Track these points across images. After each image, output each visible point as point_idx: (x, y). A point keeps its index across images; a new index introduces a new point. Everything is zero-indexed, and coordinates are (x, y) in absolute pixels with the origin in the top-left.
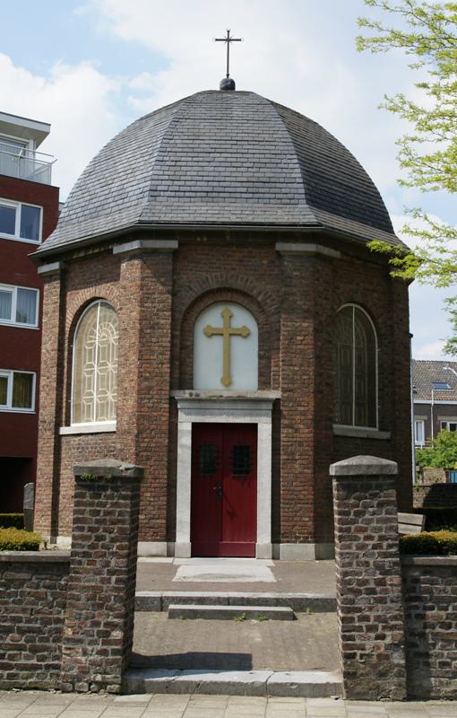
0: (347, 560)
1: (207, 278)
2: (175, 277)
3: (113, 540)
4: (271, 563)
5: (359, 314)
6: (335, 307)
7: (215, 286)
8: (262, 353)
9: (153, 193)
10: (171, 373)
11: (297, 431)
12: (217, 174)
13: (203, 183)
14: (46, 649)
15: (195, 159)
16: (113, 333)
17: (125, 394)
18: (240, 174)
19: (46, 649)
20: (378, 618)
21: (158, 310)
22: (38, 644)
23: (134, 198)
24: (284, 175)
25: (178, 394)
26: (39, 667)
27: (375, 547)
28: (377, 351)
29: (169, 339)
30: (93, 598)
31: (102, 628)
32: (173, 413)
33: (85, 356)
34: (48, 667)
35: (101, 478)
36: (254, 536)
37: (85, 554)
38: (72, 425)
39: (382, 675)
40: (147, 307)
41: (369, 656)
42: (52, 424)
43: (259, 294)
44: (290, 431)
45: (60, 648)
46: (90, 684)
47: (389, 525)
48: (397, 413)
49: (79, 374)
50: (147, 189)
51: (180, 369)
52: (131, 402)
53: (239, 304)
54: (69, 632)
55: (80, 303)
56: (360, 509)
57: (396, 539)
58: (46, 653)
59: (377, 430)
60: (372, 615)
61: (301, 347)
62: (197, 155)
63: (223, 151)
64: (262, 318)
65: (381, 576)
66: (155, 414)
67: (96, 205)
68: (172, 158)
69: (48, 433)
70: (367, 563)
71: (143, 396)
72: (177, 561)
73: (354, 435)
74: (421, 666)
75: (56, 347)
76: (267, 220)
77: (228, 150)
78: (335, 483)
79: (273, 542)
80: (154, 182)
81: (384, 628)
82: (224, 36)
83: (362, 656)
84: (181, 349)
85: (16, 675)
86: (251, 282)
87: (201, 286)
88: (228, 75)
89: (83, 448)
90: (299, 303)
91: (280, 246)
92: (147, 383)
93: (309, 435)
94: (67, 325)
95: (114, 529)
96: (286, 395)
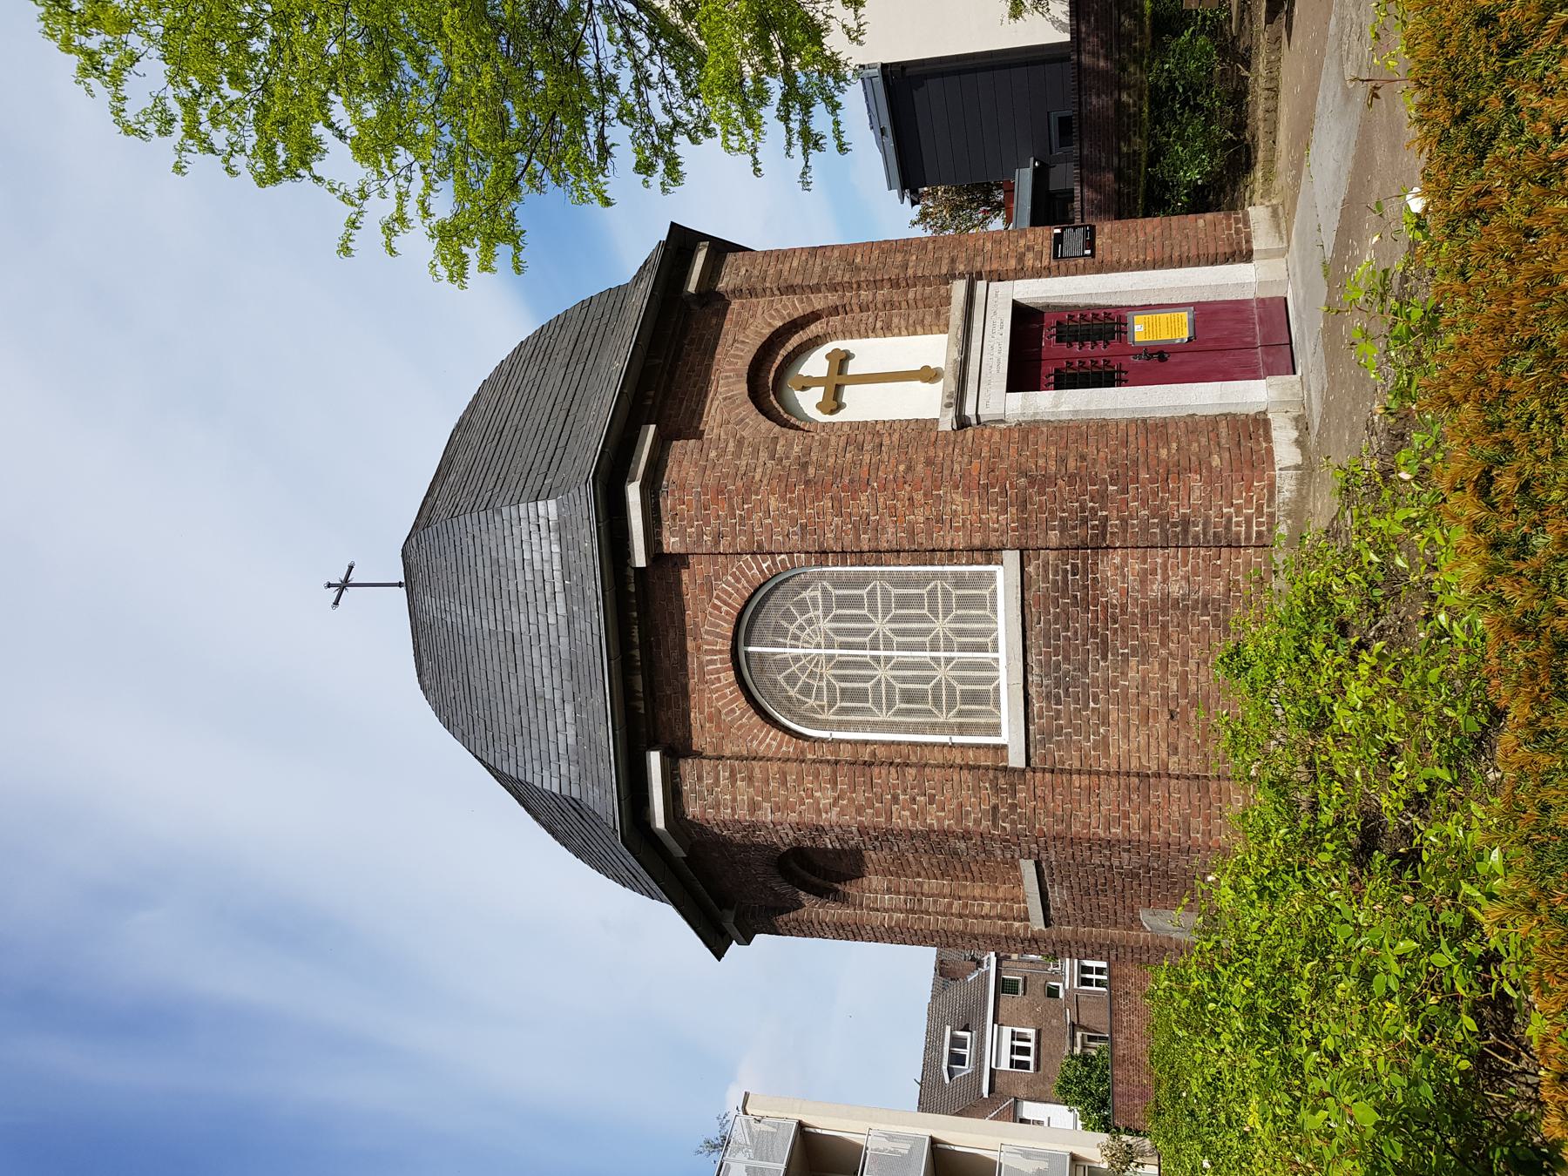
40: (764, 474)
66: (985, 450)
71: (946, 472)
92: (920, 467)
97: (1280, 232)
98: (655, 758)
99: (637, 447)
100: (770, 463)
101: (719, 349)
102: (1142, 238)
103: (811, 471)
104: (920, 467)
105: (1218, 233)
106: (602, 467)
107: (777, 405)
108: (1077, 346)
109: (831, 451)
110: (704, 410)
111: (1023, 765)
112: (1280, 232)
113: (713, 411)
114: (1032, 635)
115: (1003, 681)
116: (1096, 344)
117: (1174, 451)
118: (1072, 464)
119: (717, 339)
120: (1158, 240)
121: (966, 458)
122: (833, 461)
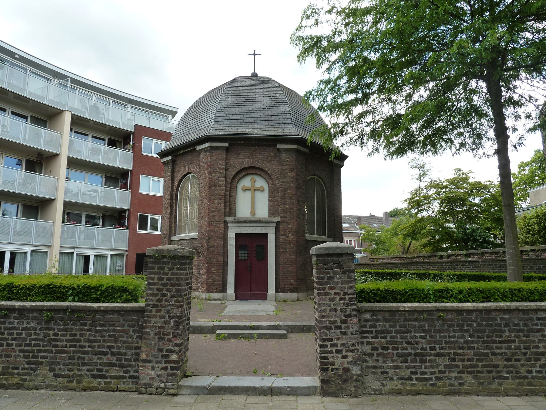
0: (323, 308)
1: (243, 162)
2: (227, 161)
3: (172, 296)
4: (275, 303)
5: (318, 181)
6: (306, 177)
7: (247, 166)
8: (270, 199)
9: (216, 120)
10: (225, 208)
11: (288, 237)
12: (248, 111)
14: (131, 366)
15: (237, 104)
16: (197, 190)
17: (202, 219)
18: (260, 112)
19: (131, 366)
20: (343, 345)
22: (123, 362)
23: (208, 123)
24: (281, 112)
25: (228, 219)
26: (124, 377)
27: (341, 299)
28: (326, 199)
29: (224, 192)
30: (159, 333)
31: (165, 353)
32: (226, 228)
33: (184, 201)
34: (130, 377)
35: (164, 257)
36: (266, 290)
37: (155, 306)
39: (345, 381)
41: (337, 369)
42: (168, 235)
43: (269, 169)
44: (285, 237)
45: (138, 365)
46: (157, 389)
47: (349, 285)
48: (336, 229)
49: (180, 210)
50: (214, 118)
51: (230, 207)
52: (205, 223)
53: (258, 174)
54: (143, 356)
55: (181, 176)
56: (331, 275)
57: (354, 294)
58: (129, 369)
59: (326, 237)
60: (339, 343)
62: (238, 102)
63: (252, 101)
64: (270, 182)
65: (345, 318)
66: (217, 229)
67: (189, 128)
69: (166, 240)
70: (336, 310)
71: (211, 220)
72: (227, 303)
73: (316, 240)
74: (370, 374)
75: (169, 197)
76: (273, 133)
77: (254, 101)
78: (314, 259)
79: (276, 292)
80: (217, 115)
81: (347, 351)
82: (253, 53)
83: (333, 369)
84: (230, 197)
85: (111, 382)
86: (265, 164)
87: (240, 166)
88: (254, 71)
90: (289, 174)
91: (279, 146)
92: (213, 214)
93: (294, 239)
95: (173, 289)
102: (288, 266)
103: (214, 188)
104: (213, 214)
109: (220, 192)
115: (188, 234)
118: (211, 249)
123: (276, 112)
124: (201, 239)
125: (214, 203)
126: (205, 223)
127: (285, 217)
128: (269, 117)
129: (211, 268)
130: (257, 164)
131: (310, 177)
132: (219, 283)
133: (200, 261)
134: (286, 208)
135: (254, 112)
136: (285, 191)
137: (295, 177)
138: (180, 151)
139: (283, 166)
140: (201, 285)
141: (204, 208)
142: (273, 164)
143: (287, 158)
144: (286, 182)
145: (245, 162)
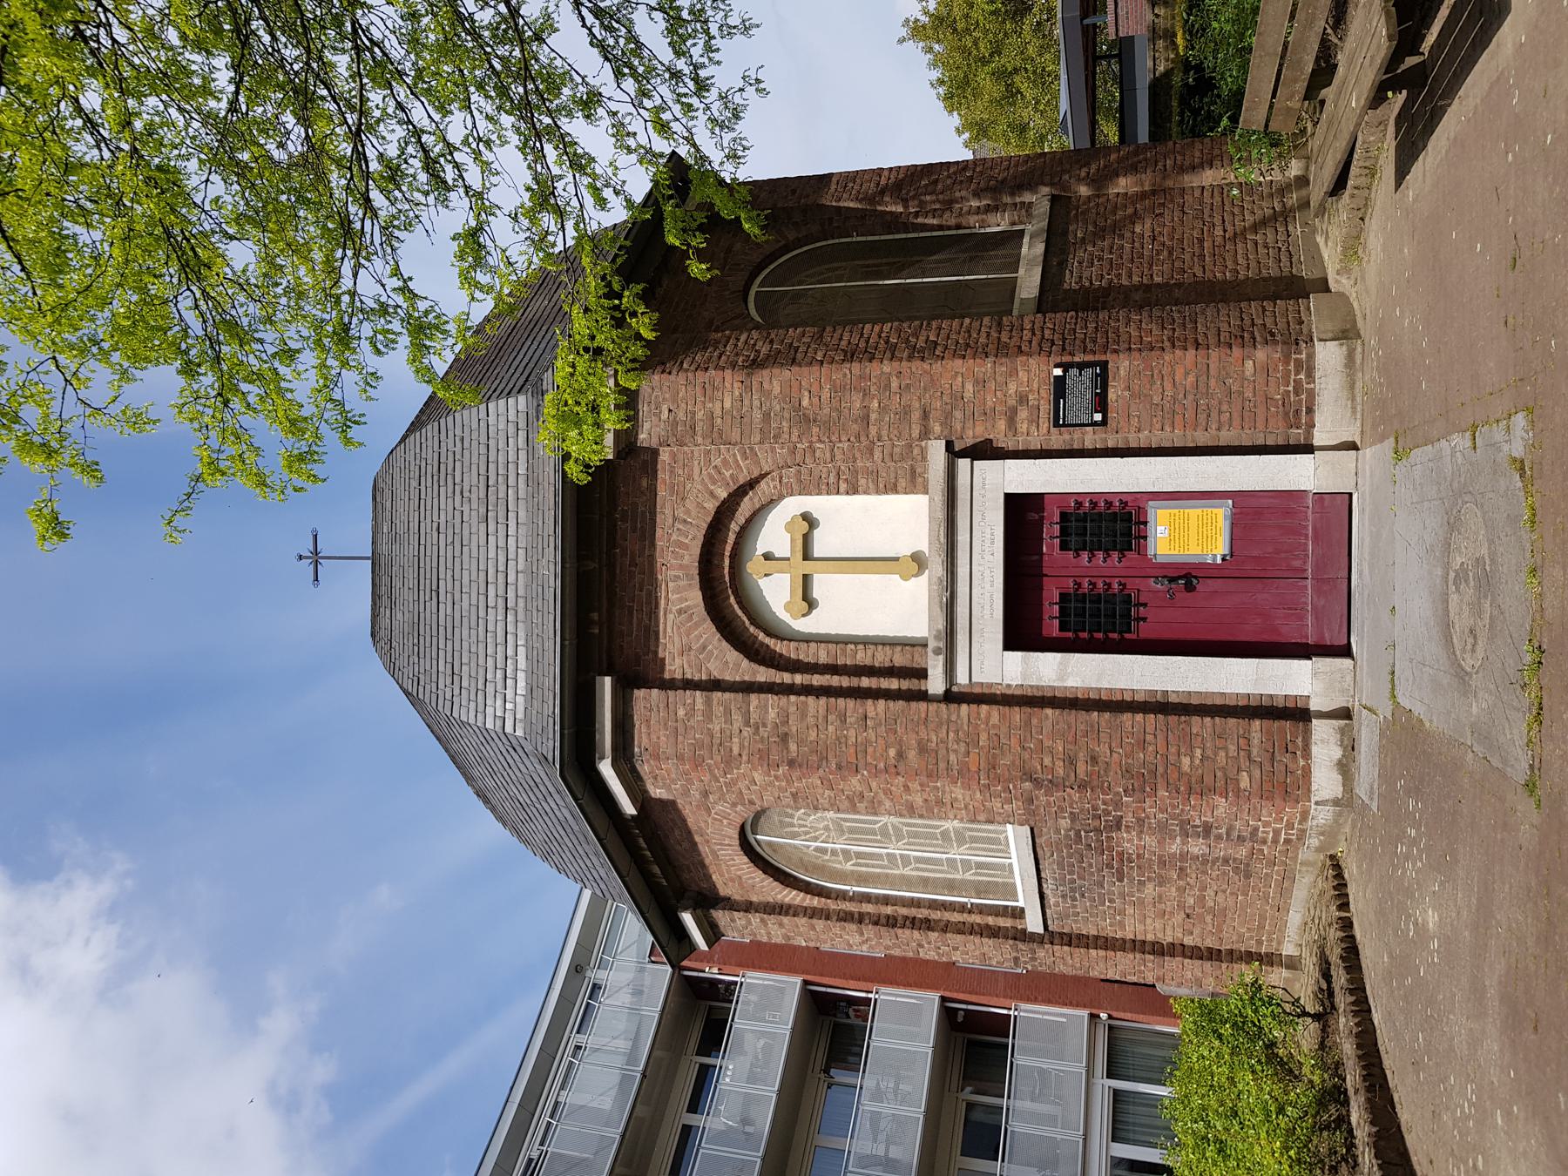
1: (680, 612)
8: (843, 486)
11: (1023, 399)
13: (491, 618)
17: (940, 803)
18: (474, 537)
21: (747, 724)
25: (936, 684)
38: (1021, 904)
40: (742, 747)
42: (1021, 945)
43: (712, 494)
44: (1023, 414)
49: (908, 882)
55: (758, 875)
61: (825, 395)
66: (984, 736)
68: (449, 681)
71: (942, 765)
75: (854, 927)
82: (306, 567)
87: (697, 625)
89: (1073, 890)
90: (727, 405)
92: (912, 755)
94: (797, 901)
96: (937, 428)
97: (1353, 399)
98: (687, 918)
99: (597, 710)
100: (747, 731)
101: (659, 532)
103: (793, 747)
104: (912, 755)
105: (1272, 389)
106: (566, 759)
107: (739, 612)
108: (1085, 555)
109: (811, 720)
110: (658, 626)
111: (1041, 930)
112: (1353, 399)
113: (669, 630)
114: (1044, 865)
115: (1014, 861)
116: (1109, 556)
117: (1197, 762)
119: (653, 513)
120: (1190, 397)
121: (963, 749)
122: (814, 734)
123: (474, 467)
124: (1034, 813)
125: (862, 748)
126: (958, 792)
127: (925, 415)
128: (492, 498)
129: (1181, 774)
130: (686, 547)
131: (753, 312)
132: (1256, 737)
133: (1140, 822)
134: (883, 409)
135: (474, 562)
136: (805, 420)
137: (739, 376)
138: (654, 875)
139: (693, 428)
140: (1267, 824)
141: (888, 792)
142: (690, 477)
143: (658, 416)
144: (767, 417)
145: (682, 600)
